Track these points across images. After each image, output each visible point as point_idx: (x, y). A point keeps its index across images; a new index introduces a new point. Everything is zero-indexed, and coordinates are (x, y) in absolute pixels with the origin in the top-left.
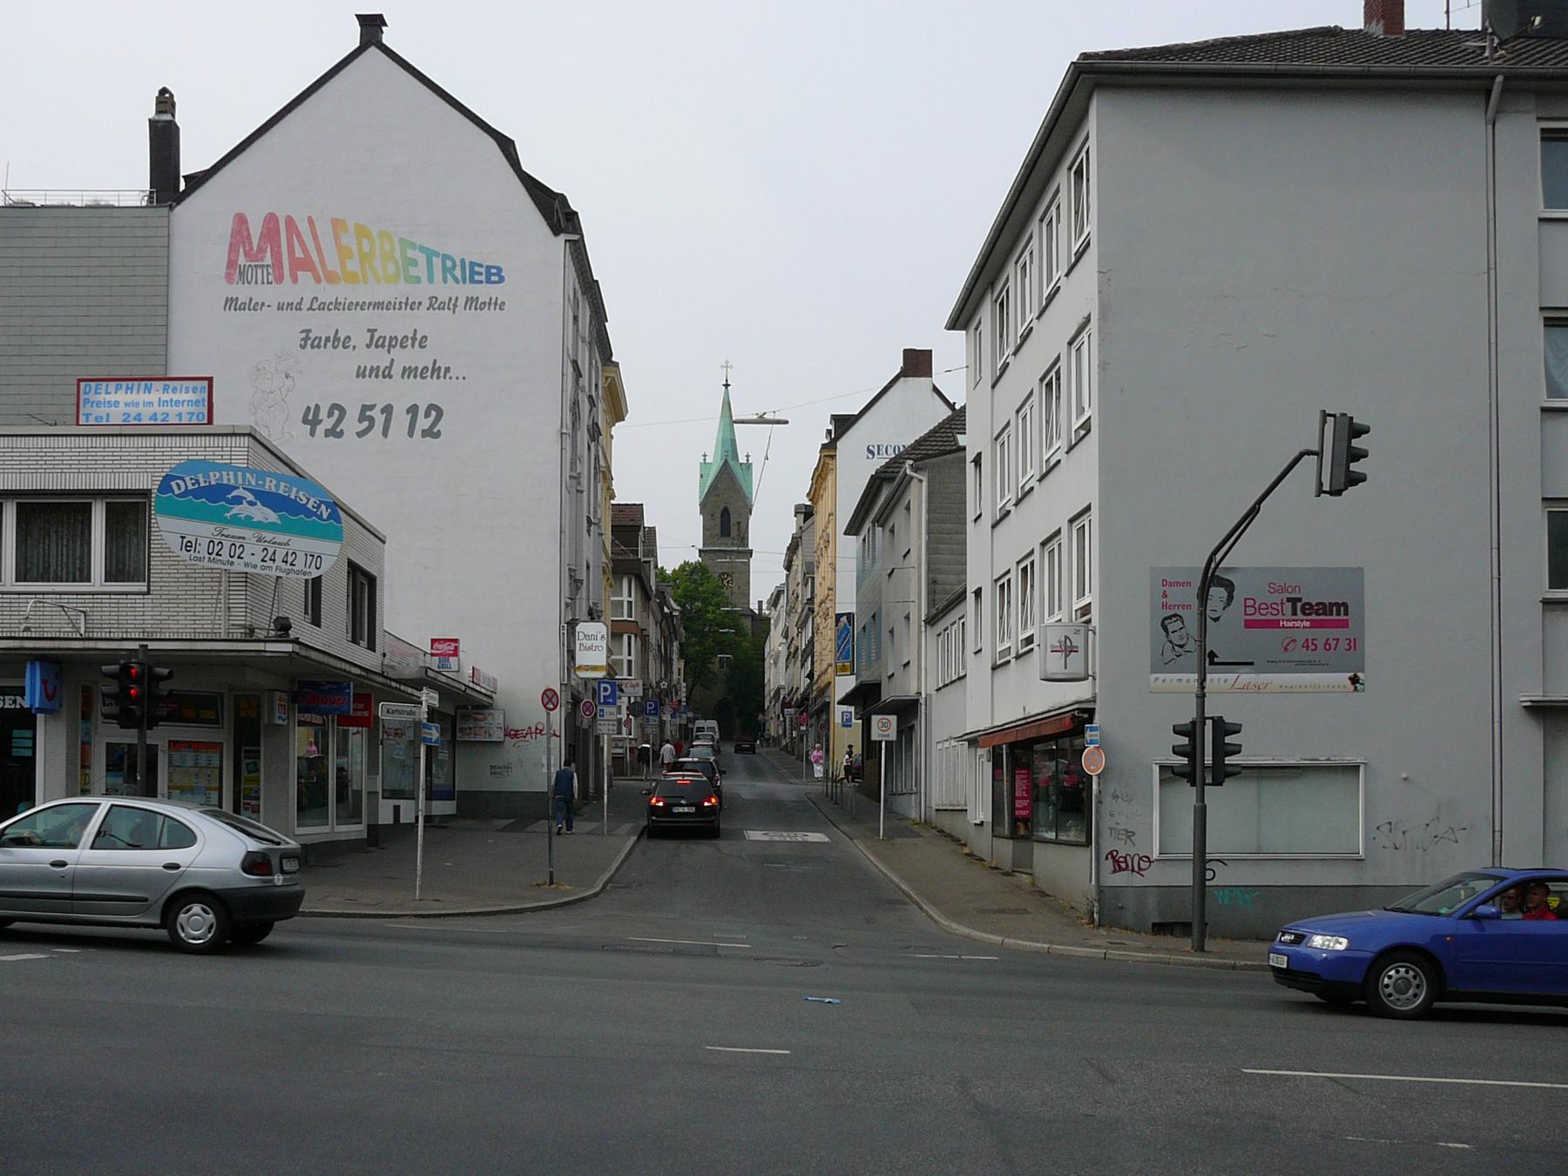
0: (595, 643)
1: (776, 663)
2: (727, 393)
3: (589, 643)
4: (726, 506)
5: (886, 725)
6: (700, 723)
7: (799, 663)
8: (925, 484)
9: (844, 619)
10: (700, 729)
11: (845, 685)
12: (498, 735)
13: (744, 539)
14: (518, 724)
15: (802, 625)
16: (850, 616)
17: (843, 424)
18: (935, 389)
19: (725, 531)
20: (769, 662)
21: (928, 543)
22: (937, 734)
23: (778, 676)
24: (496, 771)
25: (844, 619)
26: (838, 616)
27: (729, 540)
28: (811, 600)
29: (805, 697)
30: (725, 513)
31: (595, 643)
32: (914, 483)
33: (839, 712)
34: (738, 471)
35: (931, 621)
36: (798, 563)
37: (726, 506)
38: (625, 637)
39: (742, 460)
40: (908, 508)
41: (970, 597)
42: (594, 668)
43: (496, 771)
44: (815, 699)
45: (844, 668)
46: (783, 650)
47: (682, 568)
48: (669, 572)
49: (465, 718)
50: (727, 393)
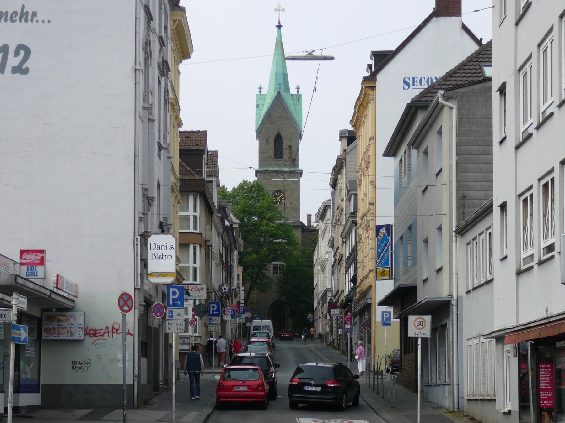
0: (165, 253)
1: (323, 269)
2: (279, 34)
3: (160, 253)
4: (279, 135)
5: (421, 324)
6: (257, 322)
7: (343, 269)
8: (455, 111)
9: (383, 230)
10: (257, 328)
11: (384, 288)
12: (79, 334)
13: (294, 161)
14: (96, 324)
15: (346, 236)
16: (388, 228)
17: (382, 59)
18: (465, 28)
19: (278, 154)
20: (317, 268)
21: (459, 163)
22: (466, 334)
23: (325, 280)
24: (76, 366)
25: (383, 230)
26: (378, 228)
27: (279, 161)
28: (354, 214)
29: (349, 300)
30: (279, 138)
31: (165, 253)
32: (445, 111)
33: (379, 312)
34: (289, 101)
35: (461, 231)
36: (342, 181)
37: (279, 135)
38: (191, 247)
39: (293, 91)
40: (440, 132)
41: (496, 210)
42: (165, 275)
43: (76, 366)
44: (358, 300)
45: (383, 273)
46: (329, 257)
47: (241, 186)
48: (229, 190)
49: (51, 319)
50: (279, 34)
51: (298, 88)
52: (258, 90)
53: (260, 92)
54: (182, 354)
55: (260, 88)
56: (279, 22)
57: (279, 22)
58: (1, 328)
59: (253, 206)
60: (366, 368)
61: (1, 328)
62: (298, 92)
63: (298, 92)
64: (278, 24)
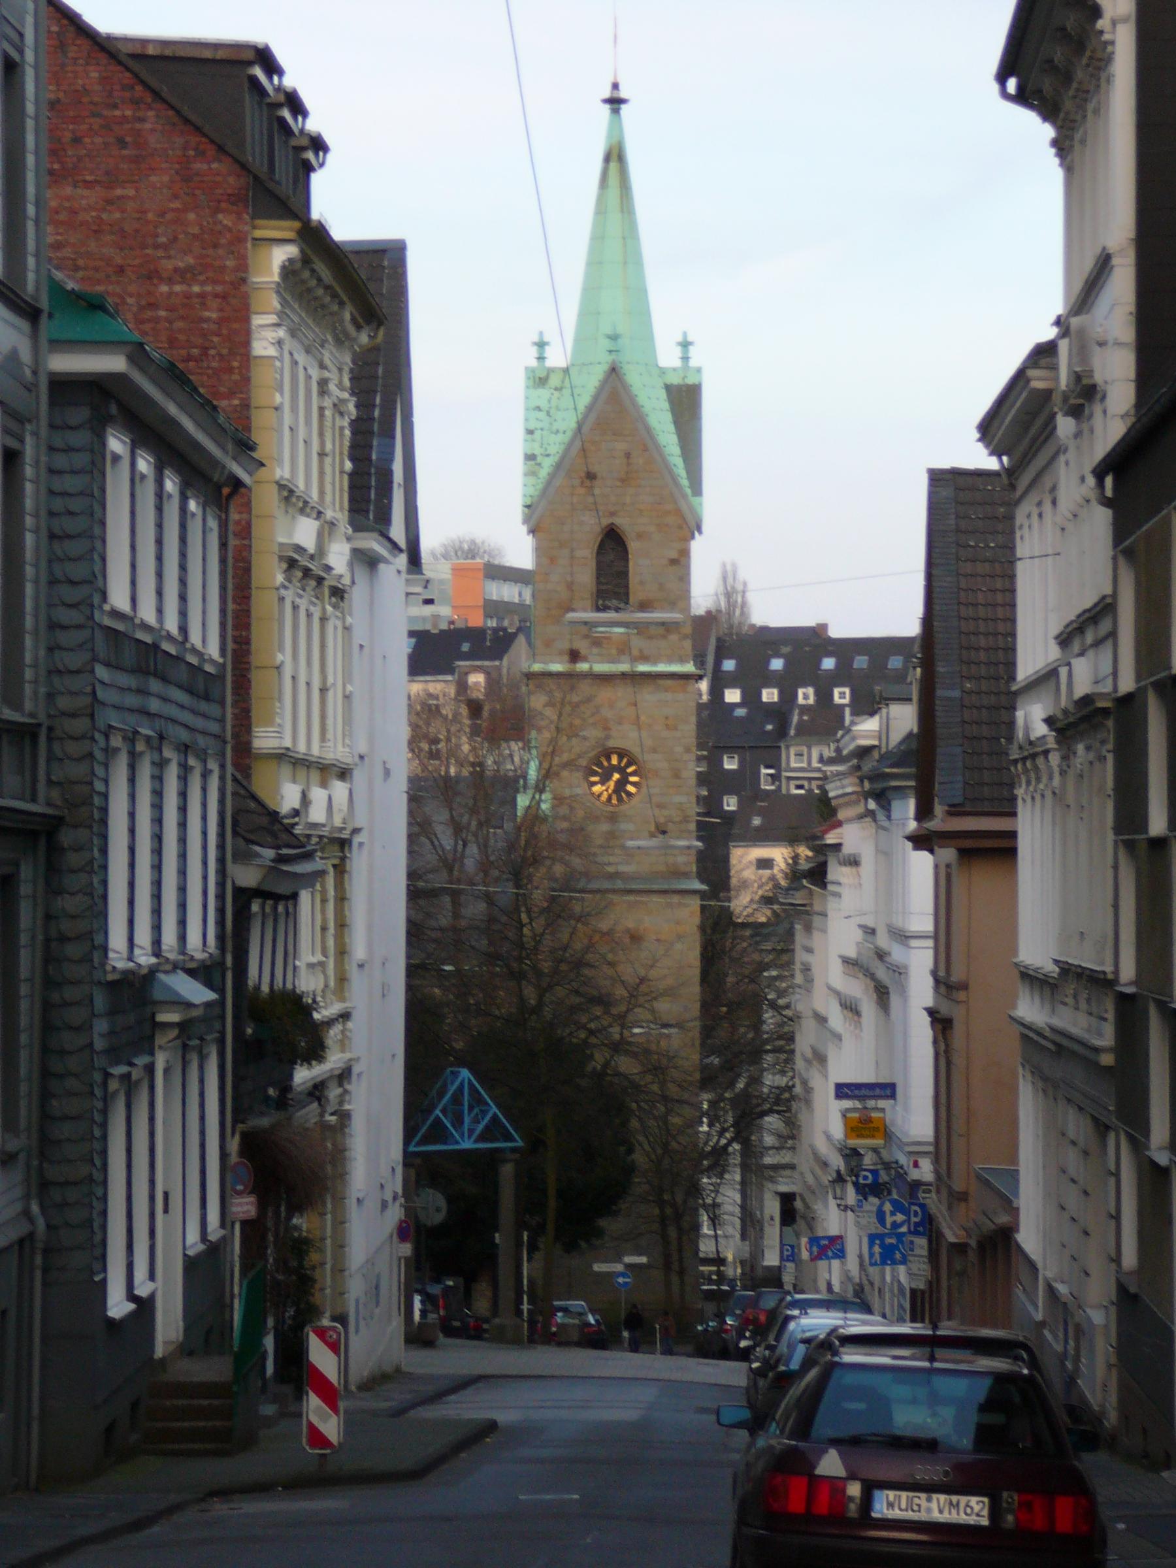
30: (613, 543)
51: (685, 345)
52: (534, 352)
53: (541, 358)
54: (598, 609)
55: (541, 345)
56: (615, 86)
57: (615, 86)
58: (9, 1159)
59: (344, 1024)
60: (908, 1433)
61: (9, 1159)
62: (685, 359)
63: (685, 359)
64: (607, 94)
